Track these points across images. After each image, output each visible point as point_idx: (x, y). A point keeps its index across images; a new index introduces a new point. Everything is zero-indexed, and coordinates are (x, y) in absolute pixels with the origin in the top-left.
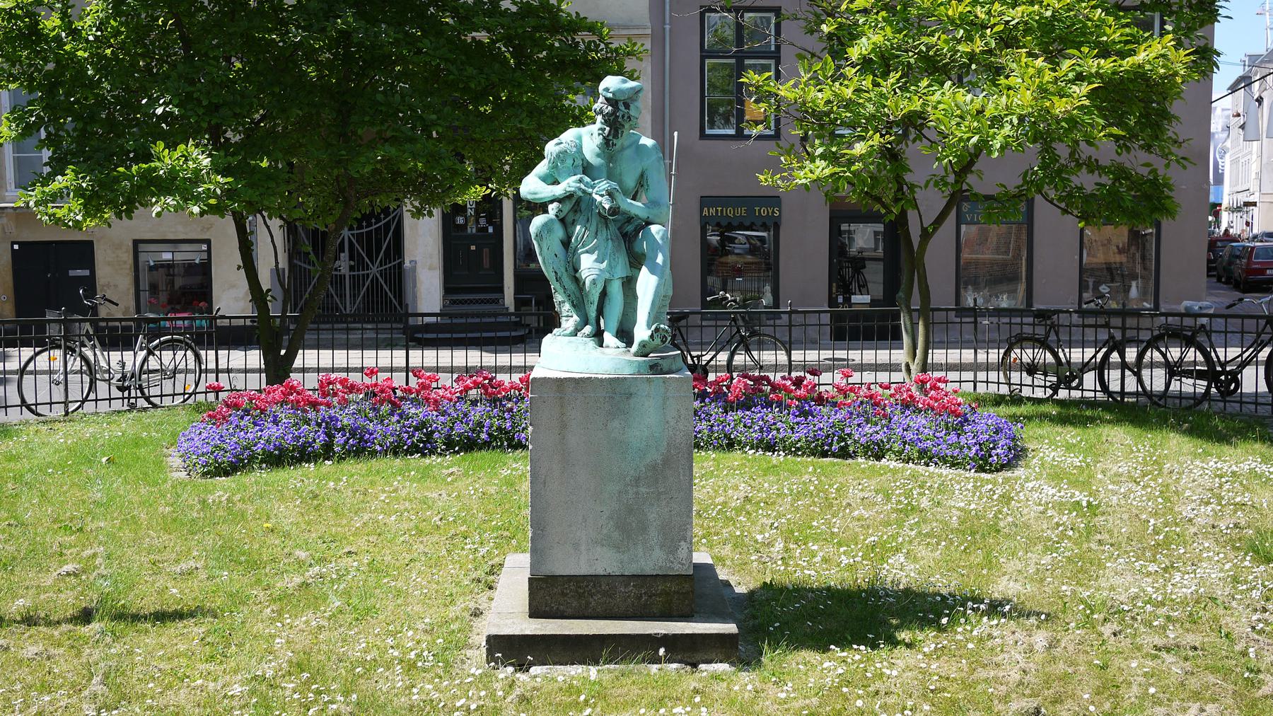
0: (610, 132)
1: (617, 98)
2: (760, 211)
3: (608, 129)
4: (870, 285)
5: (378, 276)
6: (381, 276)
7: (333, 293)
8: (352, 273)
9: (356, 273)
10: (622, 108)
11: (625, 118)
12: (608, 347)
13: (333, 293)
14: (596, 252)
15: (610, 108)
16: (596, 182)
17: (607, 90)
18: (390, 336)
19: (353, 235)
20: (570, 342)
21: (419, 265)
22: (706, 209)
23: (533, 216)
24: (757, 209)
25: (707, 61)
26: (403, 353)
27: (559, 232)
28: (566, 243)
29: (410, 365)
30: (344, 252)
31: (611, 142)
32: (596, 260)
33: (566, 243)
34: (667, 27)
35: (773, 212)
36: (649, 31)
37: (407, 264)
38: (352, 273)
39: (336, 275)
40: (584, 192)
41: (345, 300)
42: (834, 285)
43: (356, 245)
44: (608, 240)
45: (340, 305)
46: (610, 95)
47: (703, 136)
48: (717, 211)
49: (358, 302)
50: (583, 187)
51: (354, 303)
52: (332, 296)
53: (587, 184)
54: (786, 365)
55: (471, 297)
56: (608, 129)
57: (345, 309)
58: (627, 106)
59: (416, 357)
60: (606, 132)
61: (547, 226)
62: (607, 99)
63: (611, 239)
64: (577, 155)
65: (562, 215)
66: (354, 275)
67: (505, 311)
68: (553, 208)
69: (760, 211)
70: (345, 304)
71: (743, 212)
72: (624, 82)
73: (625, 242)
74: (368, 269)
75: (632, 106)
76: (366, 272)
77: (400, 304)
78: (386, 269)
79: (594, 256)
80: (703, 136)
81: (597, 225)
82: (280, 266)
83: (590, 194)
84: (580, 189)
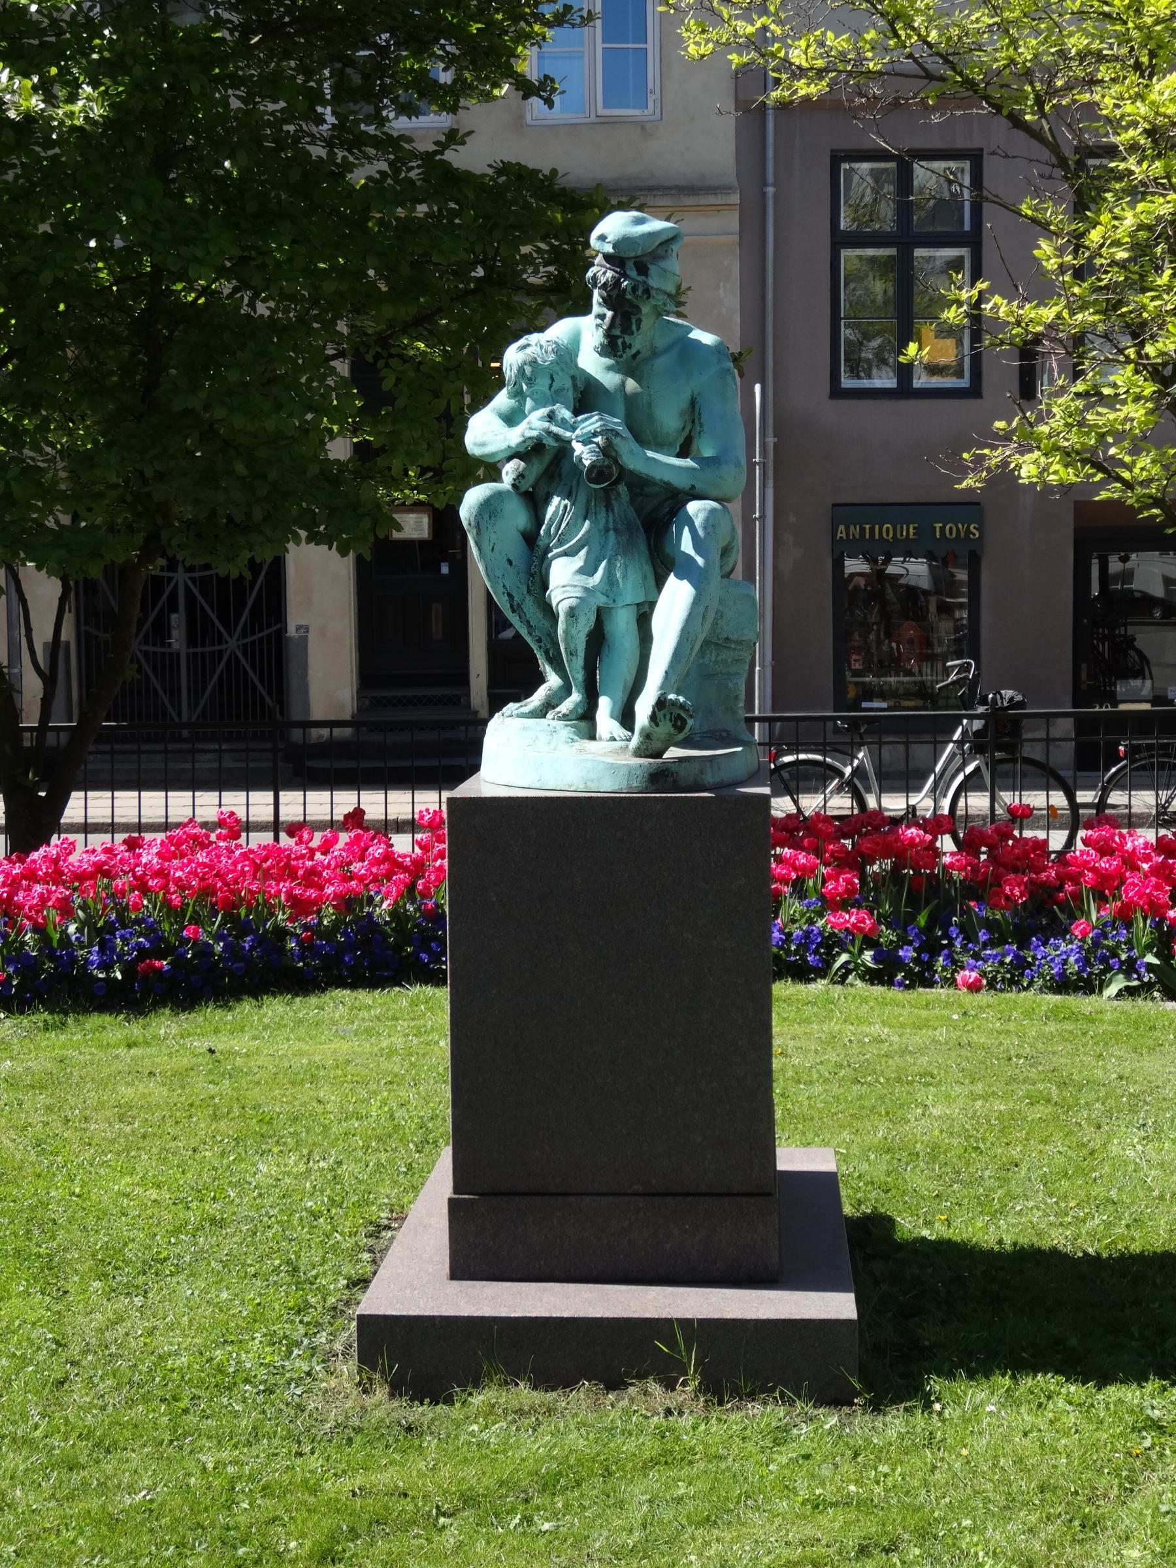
0: (613, 319)
1: (622, 255)
2: (942, 529)
3: (609, 314)
4: (1154, 670)
5: (240, 655)
6: (245, 654)
7: (158, 687)
8: (191, 650)
9: (199, 650)
10: (633, 273)
11: (640, 292)
12: (601, 739)
13: (158, 687)
14: (583, 552)
15: (610, 274)
16: (580, 418)
17: (602, 238)
18: (243, 765)
19: (193, 580)
20: (524, 729)
21: (312, 637)
22: (842, 527)
23: (463, 492)
24: (938, 526)
25: (845, 253)
26: (269, 796)
27: (519, 517)
28: (530, 538)
29: (281, 819)
30: (176, 611)
31: (620, 341)
32: (581, 571)
33: (530, 538)
34: (770, 190)
35: (968, 532)
36: (735, 199)
37: (291, 631)
38: (191, 650)
39: (163, 654)
40: (557, 437)
41: (180, 700)
42: (1084, 666)
43: (200, 598)
44: (607, 530)
45: (170, 709)
46: (609, 249)
47: (837, 392)
48: (863, 530)
49: (202, 703)
50: (555, 429)
51: (196, 705)
52: (156, 693)
53: (563, 423)
54: (986, 816)
55: (410, 693)
56: (609, 314)
57: (180, 715)
58: (642, 269)
59: (293, 804)
60: (607, 320)
61: (488, 508)
62: (607, 257)
63: (616, 530)
64: (557, 368)
65: (526, 485)
66: (195, 654)
67: (470, 717)
68: (510, 471)
69: (942, 529)
70: (180, 706)
71: (911, 530)
72: (639, 221)
73: (648, 539)
74: (220, 643)
75: (653, 269)
76: (217, 648)
77: (282, 713)
78: (253, 643)
79: (579, 561)
80: (837, 392)
81: (588, 502)
82: (63, 638)
83: (569, 442)
84: (549, 433)
